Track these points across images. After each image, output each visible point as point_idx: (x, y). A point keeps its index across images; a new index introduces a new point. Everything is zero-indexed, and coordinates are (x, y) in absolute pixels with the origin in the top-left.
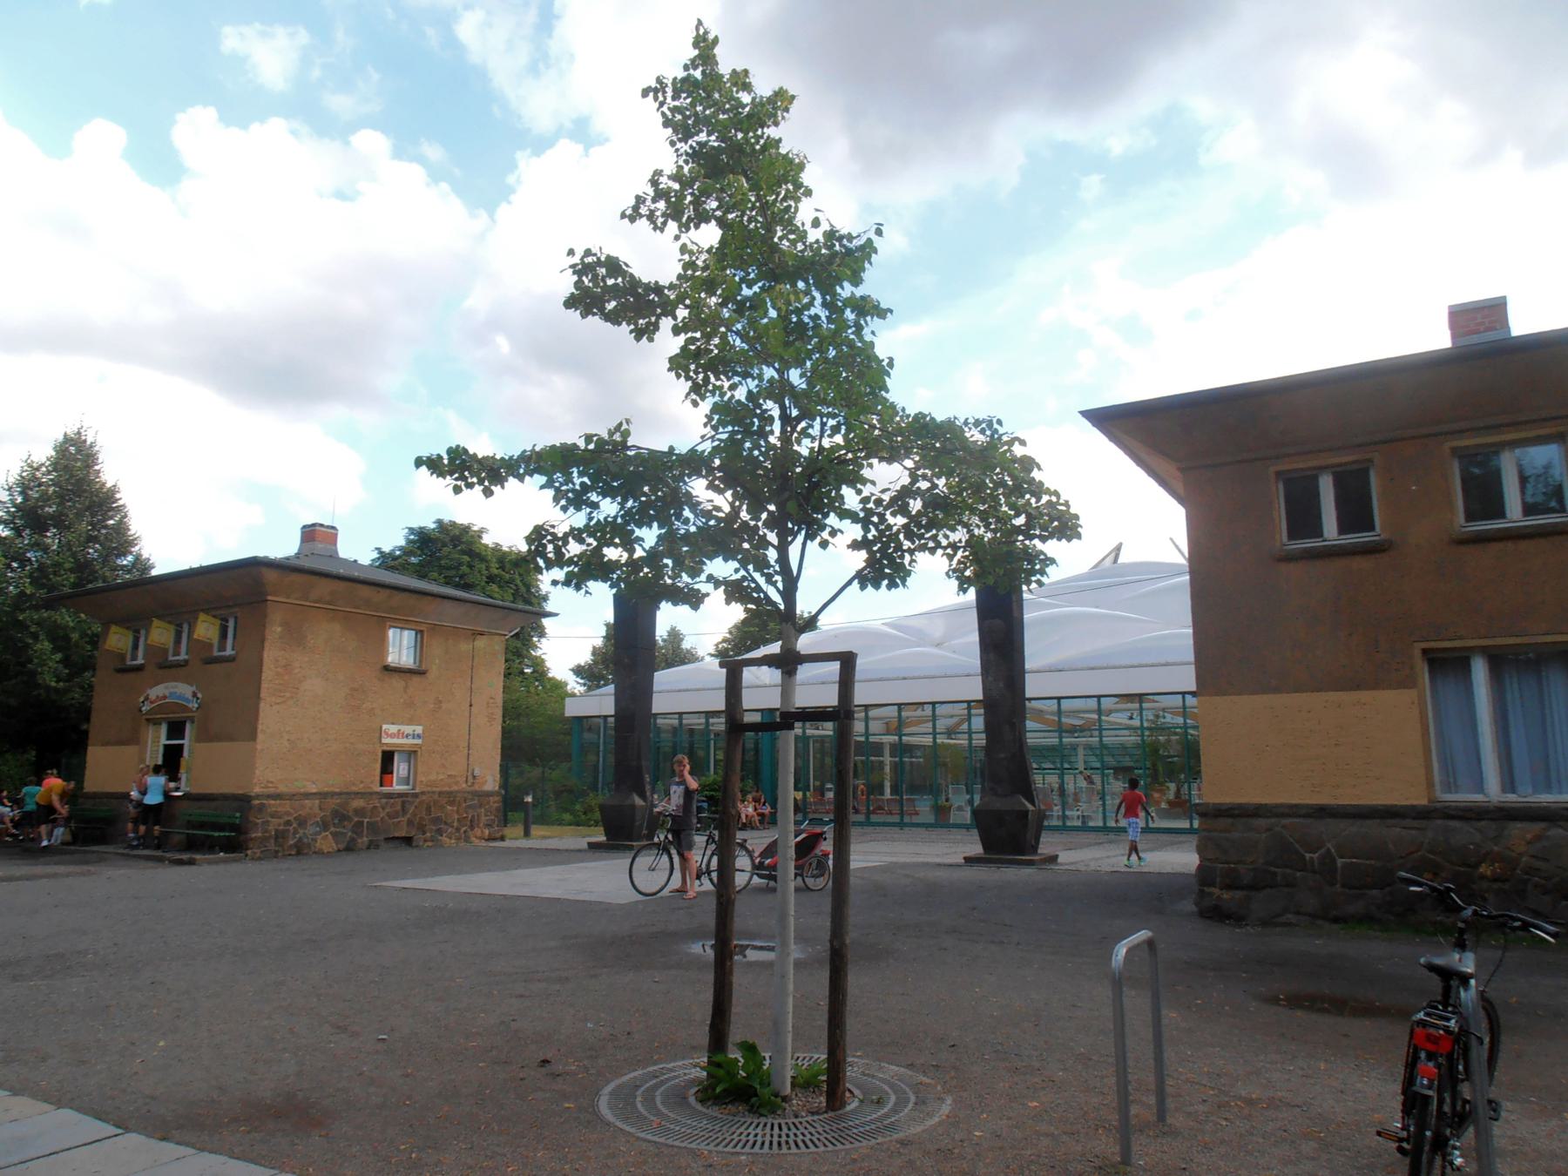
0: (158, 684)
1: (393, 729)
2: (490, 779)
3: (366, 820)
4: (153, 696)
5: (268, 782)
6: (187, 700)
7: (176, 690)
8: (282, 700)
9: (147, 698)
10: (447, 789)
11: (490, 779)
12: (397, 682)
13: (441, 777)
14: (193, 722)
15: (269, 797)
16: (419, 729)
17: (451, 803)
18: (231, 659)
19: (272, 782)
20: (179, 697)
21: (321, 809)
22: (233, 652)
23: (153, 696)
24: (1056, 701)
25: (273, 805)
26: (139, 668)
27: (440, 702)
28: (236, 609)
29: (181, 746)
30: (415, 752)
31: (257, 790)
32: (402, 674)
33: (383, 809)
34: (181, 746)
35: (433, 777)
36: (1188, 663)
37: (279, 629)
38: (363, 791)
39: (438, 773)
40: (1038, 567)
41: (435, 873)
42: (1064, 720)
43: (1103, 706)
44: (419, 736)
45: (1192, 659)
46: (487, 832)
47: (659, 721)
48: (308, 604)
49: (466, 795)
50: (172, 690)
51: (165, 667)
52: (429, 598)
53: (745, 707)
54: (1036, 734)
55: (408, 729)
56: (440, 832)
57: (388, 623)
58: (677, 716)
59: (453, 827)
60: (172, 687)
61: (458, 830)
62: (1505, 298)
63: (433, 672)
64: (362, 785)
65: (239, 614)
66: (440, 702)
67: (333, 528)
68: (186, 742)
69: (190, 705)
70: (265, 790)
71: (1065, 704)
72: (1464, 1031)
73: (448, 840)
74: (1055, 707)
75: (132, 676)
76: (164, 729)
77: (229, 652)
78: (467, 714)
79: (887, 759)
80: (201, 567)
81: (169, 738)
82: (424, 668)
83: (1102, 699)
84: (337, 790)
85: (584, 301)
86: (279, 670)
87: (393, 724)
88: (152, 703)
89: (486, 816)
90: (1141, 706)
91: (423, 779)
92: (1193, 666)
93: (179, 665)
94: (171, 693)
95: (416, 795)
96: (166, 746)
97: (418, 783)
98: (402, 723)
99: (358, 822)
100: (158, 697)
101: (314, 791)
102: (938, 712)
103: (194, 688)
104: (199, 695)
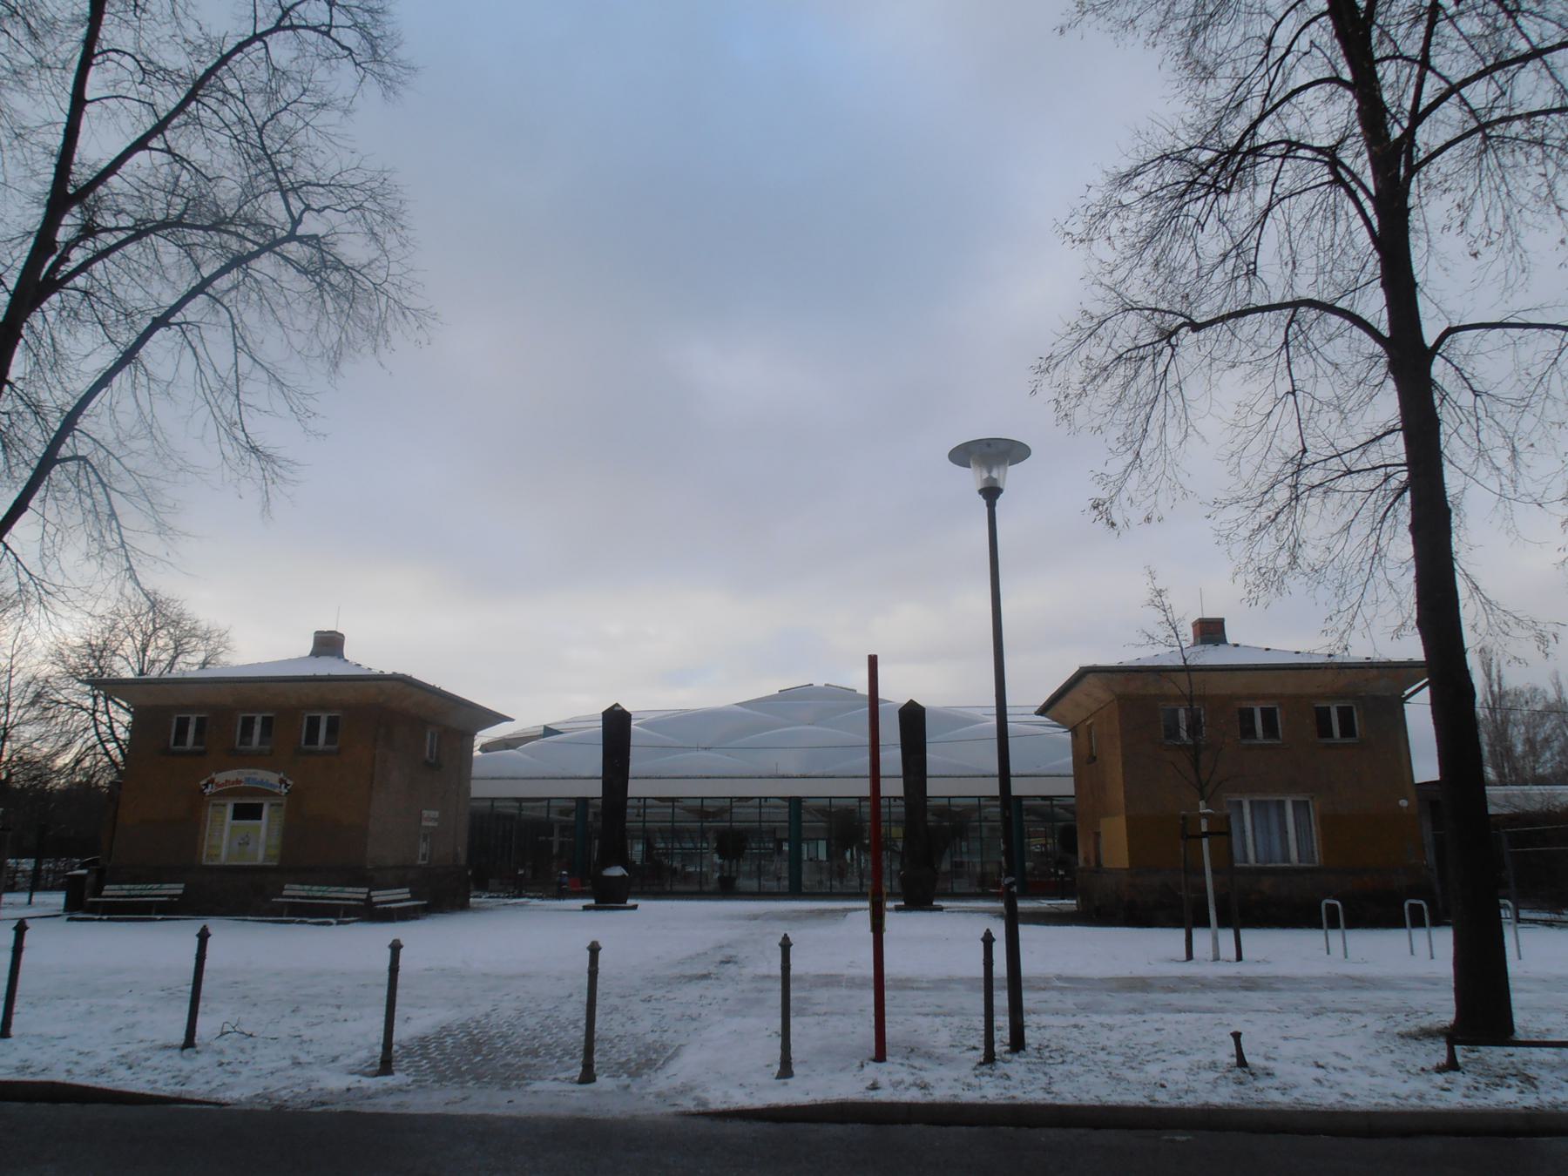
1: (426, 813)
6: (275, 787)
7: (253, 776)
9: (212, 781)
36: (931, 777)
41: (942, 900)
42: (523, 813)
45: (900, 772)
47: (1024, 803)
53: (882, 795)
54: (632, 821)
62: (1223, 619)
69: (277, 790)
71: (952, 801)
79: (556, 839)
85: (870, 657)
92: (997, 779)
100: (227, 781)
102: (551, 804)
103: (282, 775)
104: (289, 782)
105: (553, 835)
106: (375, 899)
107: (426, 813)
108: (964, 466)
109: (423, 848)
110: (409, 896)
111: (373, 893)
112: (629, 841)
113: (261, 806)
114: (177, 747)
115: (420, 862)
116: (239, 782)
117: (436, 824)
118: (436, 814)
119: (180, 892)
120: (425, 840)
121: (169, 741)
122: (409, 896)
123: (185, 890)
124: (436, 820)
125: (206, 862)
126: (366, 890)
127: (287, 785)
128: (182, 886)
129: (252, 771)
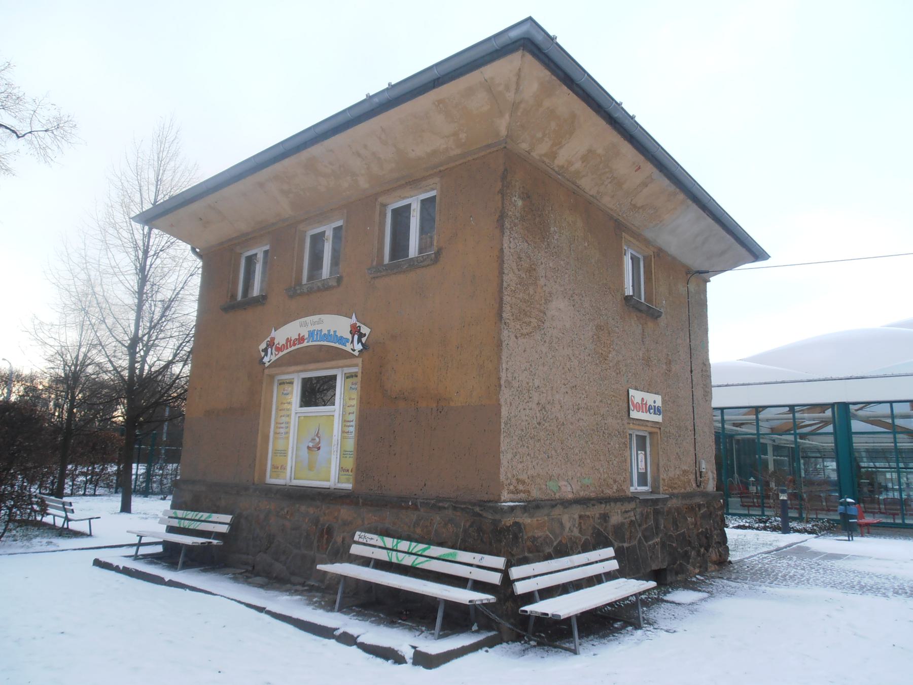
1: (637, 396)
6: (342, 340)
7: (317, 327)
9: (271, 344)
19: (523, 483)
20: (327, 337)
24: (720, 411)
26: (262, 300)
35: (671, 474)
37: (520, 203)
40: (33, 399)
43: (896, 411)
50: (311, 328)
60: (314, 323)
69: (348, 348)
72: (643, 621)
73: (692, 568)
74: (888, 411)
83: (894, 404)
88: (279, 349)
90: (757, 417)
94: (311, 334)
100: (288, 340)
103: (354, 320)
104: (365, 330)
105: (766, 454)
106: (521, 588)
107: (637, 396)
108: (539, 590)
109: (639, 462)
110: (614, 565)
111: (516, 572)
112: (146, 465)
113: (334, 378)
114: (635, 436)
115: (636, 488)
116: (301, 339)
117: (658, 418)
118: (655, 399)
119: (224, 529)
120: (642, 446)
121: (650, 439)
122: (614, 565)
123: (233, 525)
124: (657, 411)
125: (270, 480)
126: (499, 562)
127: (361, 335)
128: (228, 518)
129: (316, 318)
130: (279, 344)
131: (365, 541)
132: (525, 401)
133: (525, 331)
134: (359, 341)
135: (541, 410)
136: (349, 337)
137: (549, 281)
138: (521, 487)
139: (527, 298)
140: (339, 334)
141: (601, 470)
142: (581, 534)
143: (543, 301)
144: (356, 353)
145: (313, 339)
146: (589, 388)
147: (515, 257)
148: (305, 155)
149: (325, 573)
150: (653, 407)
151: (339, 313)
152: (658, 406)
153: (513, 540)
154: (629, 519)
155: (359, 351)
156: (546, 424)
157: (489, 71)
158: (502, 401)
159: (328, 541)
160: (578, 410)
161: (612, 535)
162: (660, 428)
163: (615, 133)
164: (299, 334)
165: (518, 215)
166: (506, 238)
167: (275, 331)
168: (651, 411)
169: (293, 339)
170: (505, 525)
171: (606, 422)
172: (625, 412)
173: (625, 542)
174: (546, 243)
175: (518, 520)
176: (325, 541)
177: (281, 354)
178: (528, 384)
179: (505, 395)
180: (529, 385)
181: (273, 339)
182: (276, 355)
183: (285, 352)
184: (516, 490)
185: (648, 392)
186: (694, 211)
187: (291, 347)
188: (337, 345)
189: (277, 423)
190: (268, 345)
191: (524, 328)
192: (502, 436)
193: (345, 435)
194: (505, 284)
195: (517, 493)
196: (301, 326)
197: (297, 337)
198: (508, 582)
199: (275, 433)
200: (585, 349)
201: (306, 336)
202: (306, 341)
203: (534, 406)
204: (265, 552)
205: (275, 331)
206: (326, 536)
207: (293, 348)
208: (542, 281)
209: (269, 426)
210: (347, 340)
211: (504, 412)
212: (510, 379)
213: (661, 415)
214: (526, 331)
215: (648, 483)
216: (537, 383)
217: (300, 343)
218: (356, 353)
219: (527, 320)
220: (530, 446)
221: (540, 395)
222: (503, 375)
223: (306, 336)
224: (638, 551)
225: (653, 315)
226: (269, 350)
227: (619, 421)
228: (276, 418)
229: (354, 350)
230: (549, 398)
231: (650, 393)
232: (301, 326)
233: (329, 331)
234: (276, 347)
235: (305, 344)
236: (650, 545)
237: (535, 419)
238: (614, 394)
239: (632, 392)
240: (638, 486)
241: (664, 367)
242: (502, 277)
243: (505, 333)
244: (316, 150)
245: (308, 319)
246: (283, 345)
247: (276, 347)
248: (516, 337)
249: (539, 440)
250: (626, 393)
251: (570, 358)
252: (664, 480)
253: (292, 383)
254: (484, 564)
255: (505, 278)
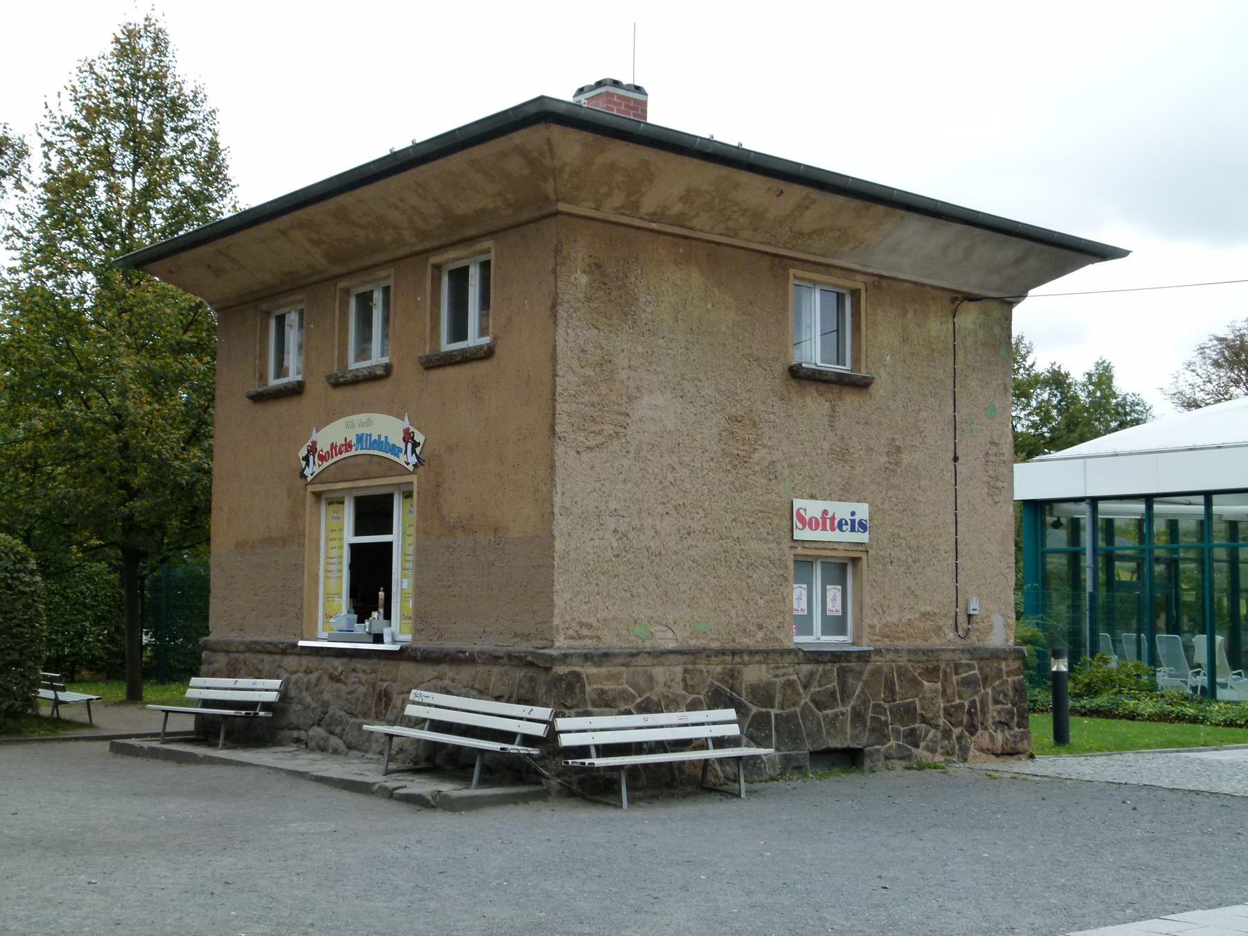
0: (329, 422)
1: (811, 508)
2: (998, 621)
3: (773, 712)
4: (323, 446)
5: (581, 624)
6: (394, 450)
7: (366, 430)
8: (600, 439)
9: (313, 449)
10: (920, 644)
11: (998, 621)
12: (815, 404)
13: (908, 616)
14: (408, 495)
15: (587, 657)
16: (862, 511)
17: (932, 673)
18: (486, 354)
19: (590, 626)
21: (686, 687)
22: (486, 340)
23: (323, 446)
25: (598, 676)
26: (296, 390)
27: (899, 450)
28: (488, 244)
29: (390, 544)
30: (855, 561)
31: (562, 643)
32: (822, 387)
33: (806, 687)
34: (390, 544)
37: (584, 279)
38: (763, 646)
39: (902, 609)
44: (863, 526)
46: (999, 737)
48: (637, 222)
49: (956, 656)
50: (360, 431)
51: (347, 384)
52: (881, 209)
55: (841, 510)
56: (913, 738)
57: (792, 271)
58: (1201, 499)
59: (936, 727)
60: (362, 425)
61: (947, 734)
63: (880, 389)
64: (760, 635)
65: (492, 256)
66: (899, 450)
67: (638, 89)
68: (394, 538)
69: (401, 460)
70: (577, 643)
75: (283, 408)
76: (348, 514)
77: (474, 339)
78: (949, 476)
80: (416, 146)
81: (358, 532)
82: (863, 373)
84: (715, 645)
86: (589, 372)
87: (812, 497)
88: (322, 458)
89: (996, 702)
91: (875, 621)
93: (372, 378)
94: (360, 438)
95: (863, 657)
96: (354, 548)
97: (866, 630)
98: (829, 497)
99: (759, 715)
101: (672, 645)
104: (419, 438)
106: (566, 740)
111: (561, 724)
119: (272, 697)
123: (284, 694)
126: (544, 713)
127: (415, 445)
128: (276, 683)
129: (363, 417)
130: (322, 450)
131: (420, 700)
132: (593, 529)
133: (592, 443)
134: (413, 451)
135: (621, 539)
136: (402, 445)
137: (636, 371)
138: (585, 632)
139: (596, 399)
140: (391, 441)
141: (733, 613)
142: (687, 691)
143: (625, 399)
144: (410, 468)
145: (362, 446)
146: (710, 505)
147: (577, 352)
148: (332, 204)
149: (372, 733)
150: (849, 522)
151: (389, 413)
152: (804, 528)
153: (566, 690)
154: (785, 678)
155: (414, 465)
156: (628, 556)
157: (518, 137)
158: (556, 533)
159: (387, 705)
160: (689, 534)
161: (747, 696)
162: (867, 551)
163: (718, 166)
164: (346, 439)
165: (581, 296)
166: (561, 331)
167: (317, 432)
168: (844, 528)
169: (338, 445)
170: (556, 672)
171: (743, 547)
172: (785, 532)
173: (773, 707)
174: (630, 322)
175: (577, 669)
176: (383, 706)
177: (326, 464)
178: (598, 508)
179: (561, 524)
180: (600, 509)
181: (314, 443)
182: (320, 466)
183: (331, 461)
184: (578, 635)
185: (840, 500)
186: (915, 226)
187: (336, 455)
188: (389, 456)
189: (328, 558)
190: (309, 451)
191: (591, 439)
192: (556, 573)
193: (329, 574)
194: (559, 389)
195: (580, 638)
196: (347, 427)
197: (344, 443)
198: (553, 734)
199: (326, 571)
200: (703, 453)
201: (354, 442)
202: (354, 448)
203: (608, 535)
204: (319, 725)
205: (317, 432)
206: (384, 699)
207: (340, 457)
208: (623, 375)
209: (318, 562)
210: (400, 450)
211: (559, 545)
212: (568, 504)
213: (867, 532)
214: (595, 442)
215: (849, 630)
216: (613, 505)
217: (347, 451)
218: (410, 468)
219: (597, 428)
220: (601, 583)
221: (618, 520)
222: (558, 500)
223: (354, 442)
224: (801, 721)
225: (860, 385)
226: (311, 458)
227: (773, 545)
228: (326, 551)
229: (408, 464)
230: (636, 522)
231: (844, 501)
232: (347, 427)
233: (379, 436)
234: (319, 455)
235: (353, 452)
236: (827, 716)
237: (610, 551)
238: (761, 509)
239: (798, 504)
240: (824, 633)
241: (884, 459)
242: (555, 381)
243: (560, 450)
244: (345, 199)
245: (355, 418)
246: (328, 452)
247: (319, 455)
248: (578, 452)
249: (616, 576)
250: (789, 506)
251: (673, 468)
252: (872, 627)
253: (342, 503)
254: (533, 716)
255: (559, 381)
